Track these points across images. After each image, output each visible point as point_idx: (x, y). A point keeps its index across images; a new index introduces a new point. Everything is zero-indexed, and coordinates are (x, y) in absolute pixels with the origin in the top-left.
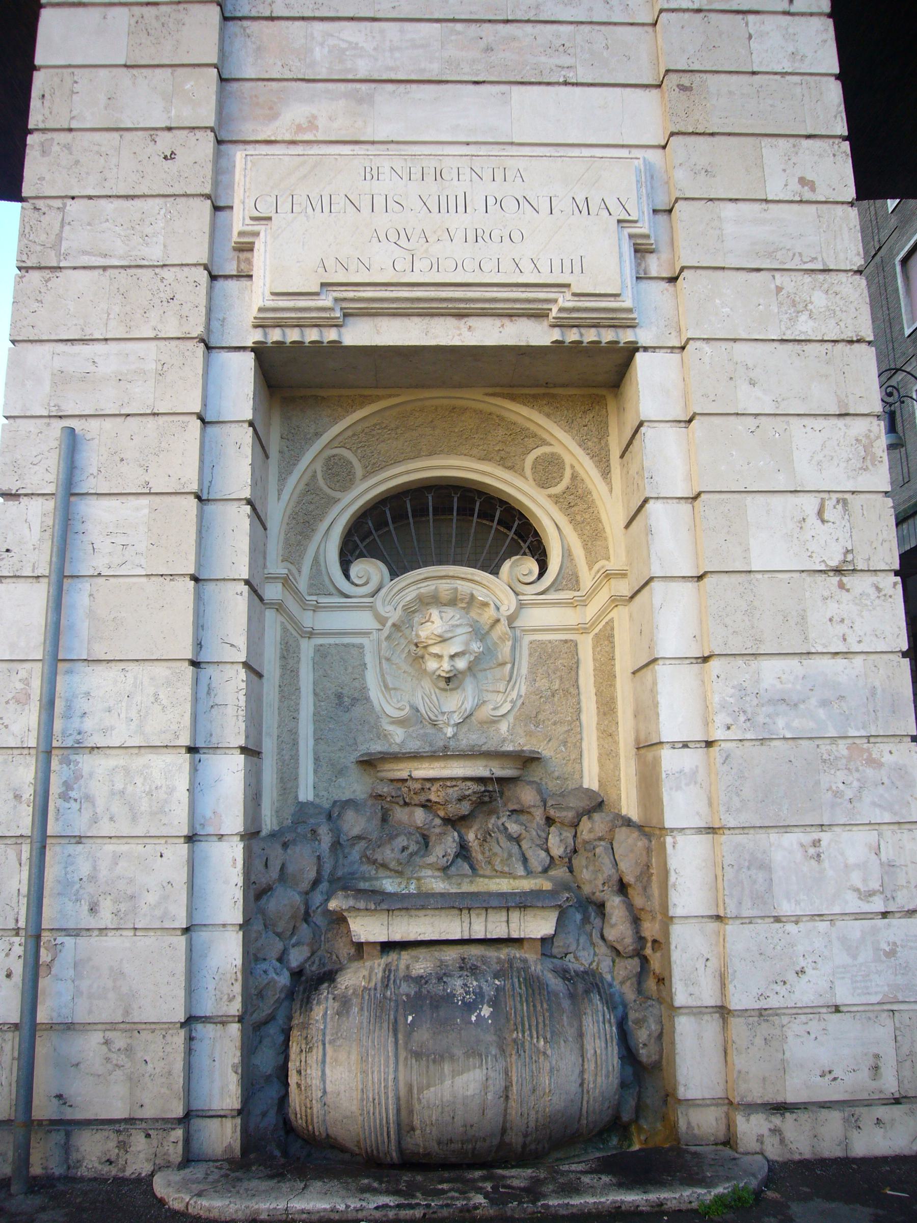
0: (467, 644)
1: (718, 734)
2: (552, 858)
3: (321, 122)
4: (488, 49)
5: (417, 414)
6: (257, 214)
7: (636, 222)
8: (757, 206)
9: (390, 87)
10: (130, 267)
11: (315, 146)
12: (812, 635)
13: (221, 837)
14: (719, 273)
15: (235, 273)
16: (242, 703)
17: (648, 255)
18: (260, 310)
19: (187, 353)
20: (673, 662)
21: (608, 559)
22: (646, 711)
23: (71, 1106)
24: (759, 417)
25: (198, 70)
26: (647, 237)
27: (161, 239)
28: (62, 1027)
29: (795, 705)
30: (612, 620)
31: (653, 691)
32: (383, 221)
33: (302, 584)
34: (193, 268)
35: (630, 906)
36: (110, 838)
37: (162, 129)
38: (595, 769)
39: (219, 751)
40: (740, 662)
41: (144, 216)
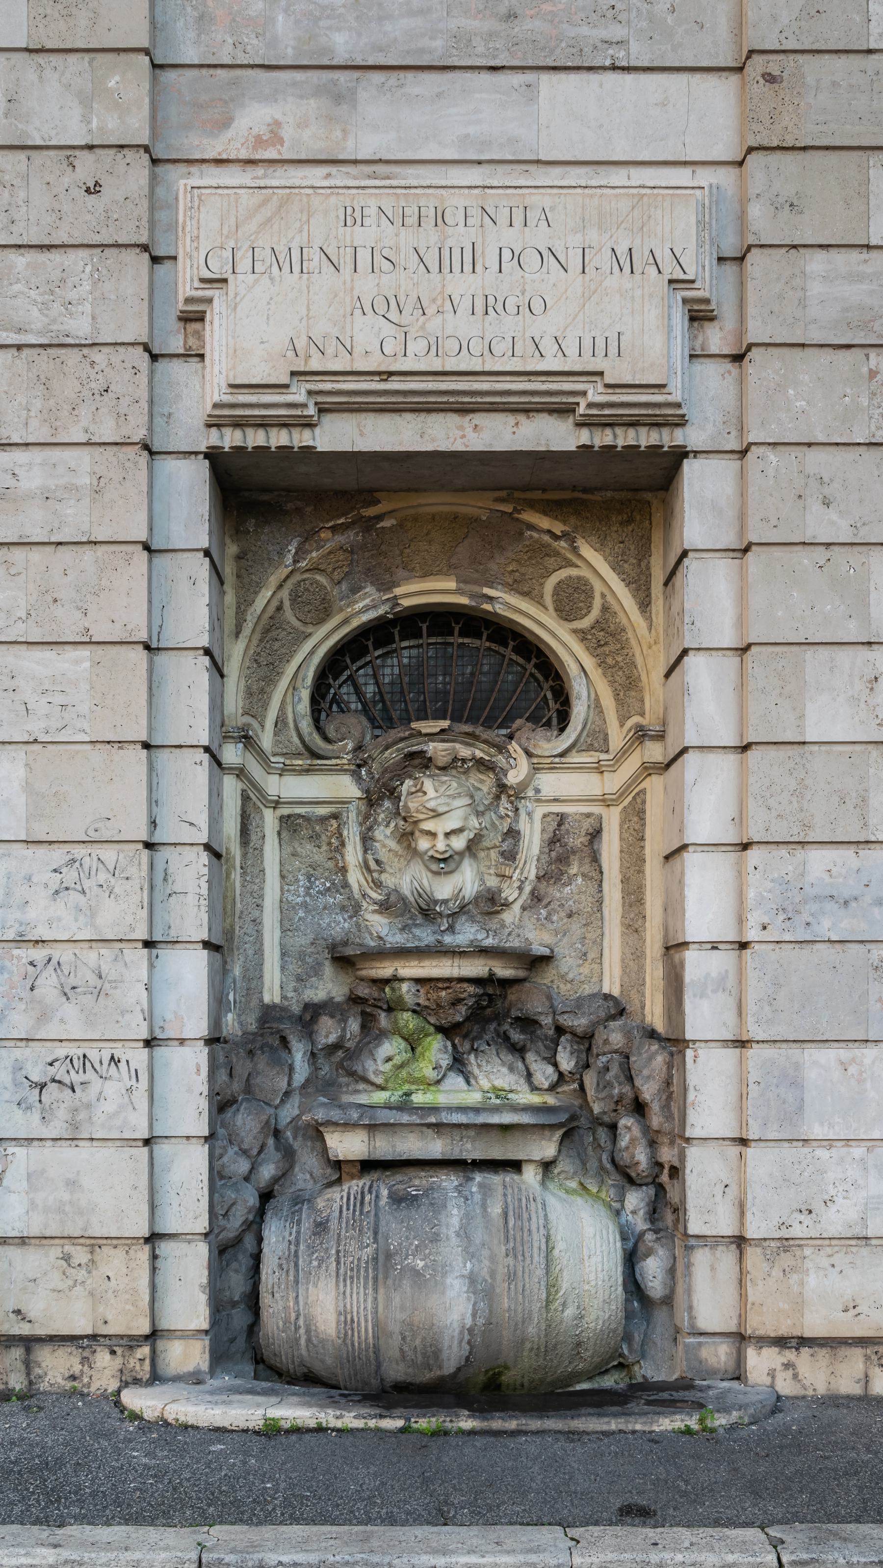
0: (466, 819)
1: (752, 935)
2: (561, 1074)
3: (287, 133)
4: (510, 16)
5: (409, 525)
6: (208, 275)
7: (693, 282)
8: (855, 256)
9: (377, 77)
10: (50, 346)
11: (280, 171)
12: (873, 821)
13: (182, 1041)
14: (798, 353)
15: (182, 351)
16: (204, 891)
17: (706, 324)
18: (215, 406)
19: (127, 464)
20: (706, 848)
21: (642, 714)
22: (674, 906)
23: (30, 1321)
24: (832, 547)
25: (123, 56)
26: (707, 301)
27: (87, 307)
28: (17, 1241)
29: (846, 903)
30: (643, 791)
31: (681, 882)
32: (367, 286)
33: (267, 741)
34: (130, 348)
35: (646, 1129)
36: (61, 1041)
37: (82, 148)
38: (617, 971)
39: (178, 946)
40: (783, 851)
41: (64, 275)
